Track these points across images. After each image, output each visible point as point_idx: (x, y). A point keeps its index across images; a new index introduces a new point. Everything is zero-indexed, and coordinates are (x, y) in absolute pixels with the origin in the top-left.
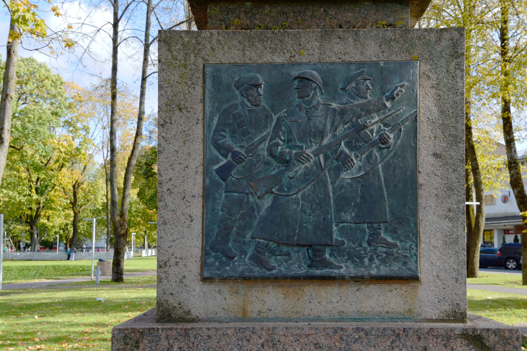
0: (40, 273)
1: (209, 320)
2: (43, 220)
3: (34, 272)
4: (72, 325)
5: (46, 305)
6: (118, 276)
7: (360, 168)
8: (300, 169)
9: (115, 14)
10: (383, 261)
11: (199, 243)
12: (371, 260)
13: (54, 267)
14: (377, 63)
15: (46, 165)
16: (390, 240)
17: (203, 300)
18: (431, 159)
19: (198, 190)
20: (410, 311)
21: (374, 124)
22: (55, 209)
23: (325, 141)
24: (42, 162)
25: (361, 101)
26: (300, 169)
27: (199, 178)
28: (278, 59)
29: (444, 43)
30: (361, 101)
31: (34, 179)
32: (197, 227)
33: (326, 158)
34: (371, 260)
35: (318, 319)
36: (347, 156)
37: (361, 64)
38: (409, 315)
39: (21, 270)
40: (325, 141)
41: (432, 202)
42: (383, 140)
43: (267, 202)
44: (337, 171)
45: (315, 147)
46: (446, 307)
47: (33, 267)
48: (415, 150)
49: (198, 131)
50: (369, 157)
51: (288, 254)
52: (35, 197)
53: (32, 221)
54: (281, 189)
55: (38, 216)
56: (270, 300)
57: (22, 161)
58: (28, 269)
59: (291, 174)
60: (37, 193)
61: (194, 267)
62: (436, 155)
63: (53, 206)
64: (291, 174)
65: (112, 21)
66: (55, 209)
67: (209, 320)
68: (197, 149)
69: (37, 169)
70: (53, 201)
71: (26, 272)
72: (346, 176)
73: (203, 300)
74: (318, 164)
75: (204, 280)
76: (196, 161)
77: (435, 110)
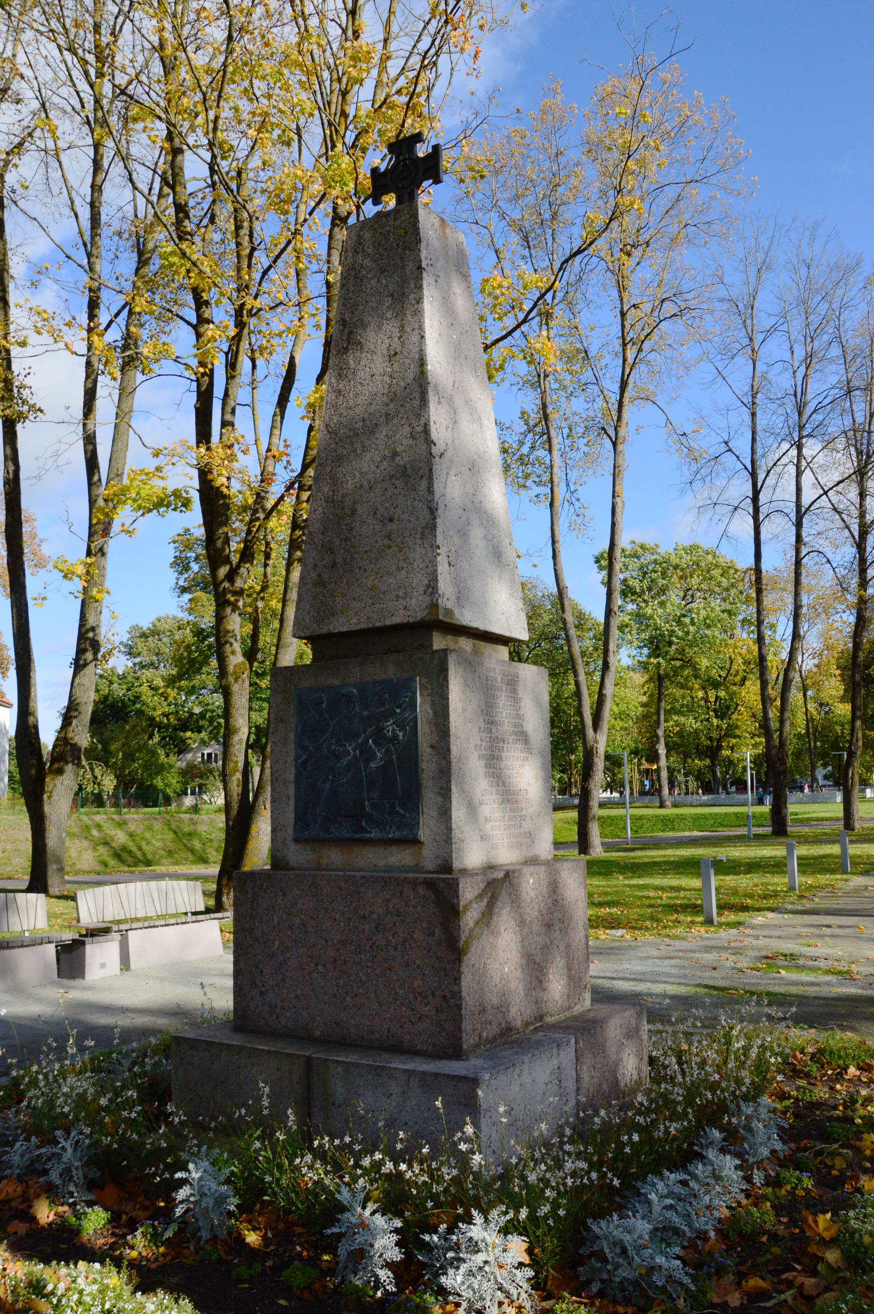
0: (721, 821)
1: (300, 869)
2: (725, 753)
3: (712, 822)
4: (678, 889)
5: (646, 864)
6: (779, 826)
7: (381, 759)
8: (345, 761)
9: (754, 485)
10: (398, 828)
11: (293, 815)
12: (391, 827)
13: (736, 815)
14: (392, 680)
15: (725, 679)
16: (402, 812)
17: (296, 855)
18: (429, 750)
19: (292, 777)
20: (417, 865)
21: (390, 727)
22: (739, 737)
23: (360, 741)
24: (720, 676)
25: (382, 709)
26: (345, 761)
27: (293, 770)
28: (336, 682)
29: (435, 661)
30: (382, 709)
31: (712, 700)
32: (292, 803)
33: (361, 753)
34: (391, 827)
35: (361, 870)
36: (373, 751)
37: (383, 682)
38: (417, 868)
39: (697, 818)
40: (360, 741)
41: (430, 783)
42: (395, 737)
43: (327, 786)
44: (367, 761)
45: (354, 745)
46: (439, 862)
47: (710, 814)
48: (416, 742)
49: (292, 736)
50: (386, 751)
51: (340, 823)
52: (715, 721)
53: (712, 752)
54: (334, 777)
55: (720, 747)
56: (334, 856)
57: (696, 677)
58: (705, 817)
59: (339, 765)
60: (717, 717)
61: (290, 831)
62: (432, 747)
63: (737, 732)
64: (339, 765)
65: (750, 494)
66: (739, 737)
67: (300, 869)
68: (291, 747)
69: (716, 685)
70: (737, 727)
71: (702, 822)
72: (373, 765)
73: (296, 855)
74: (355, 756)
75: (297, 841)
76: (291, 759)
77: (430, 711)
